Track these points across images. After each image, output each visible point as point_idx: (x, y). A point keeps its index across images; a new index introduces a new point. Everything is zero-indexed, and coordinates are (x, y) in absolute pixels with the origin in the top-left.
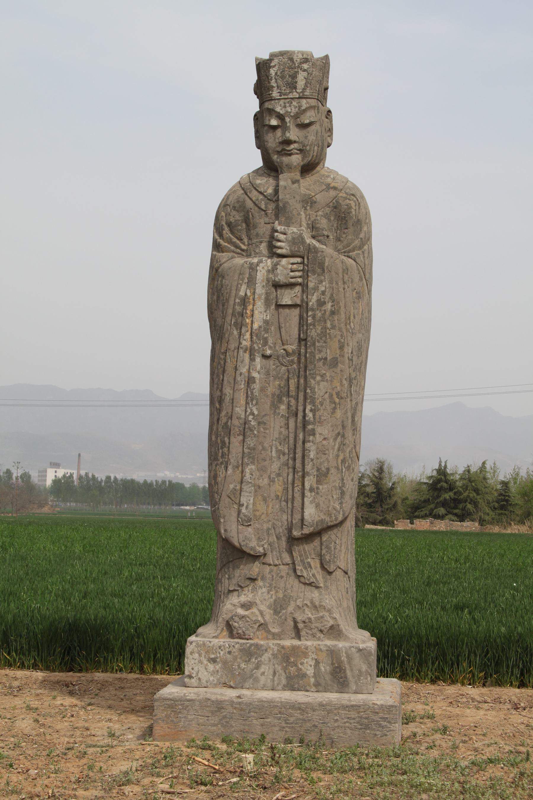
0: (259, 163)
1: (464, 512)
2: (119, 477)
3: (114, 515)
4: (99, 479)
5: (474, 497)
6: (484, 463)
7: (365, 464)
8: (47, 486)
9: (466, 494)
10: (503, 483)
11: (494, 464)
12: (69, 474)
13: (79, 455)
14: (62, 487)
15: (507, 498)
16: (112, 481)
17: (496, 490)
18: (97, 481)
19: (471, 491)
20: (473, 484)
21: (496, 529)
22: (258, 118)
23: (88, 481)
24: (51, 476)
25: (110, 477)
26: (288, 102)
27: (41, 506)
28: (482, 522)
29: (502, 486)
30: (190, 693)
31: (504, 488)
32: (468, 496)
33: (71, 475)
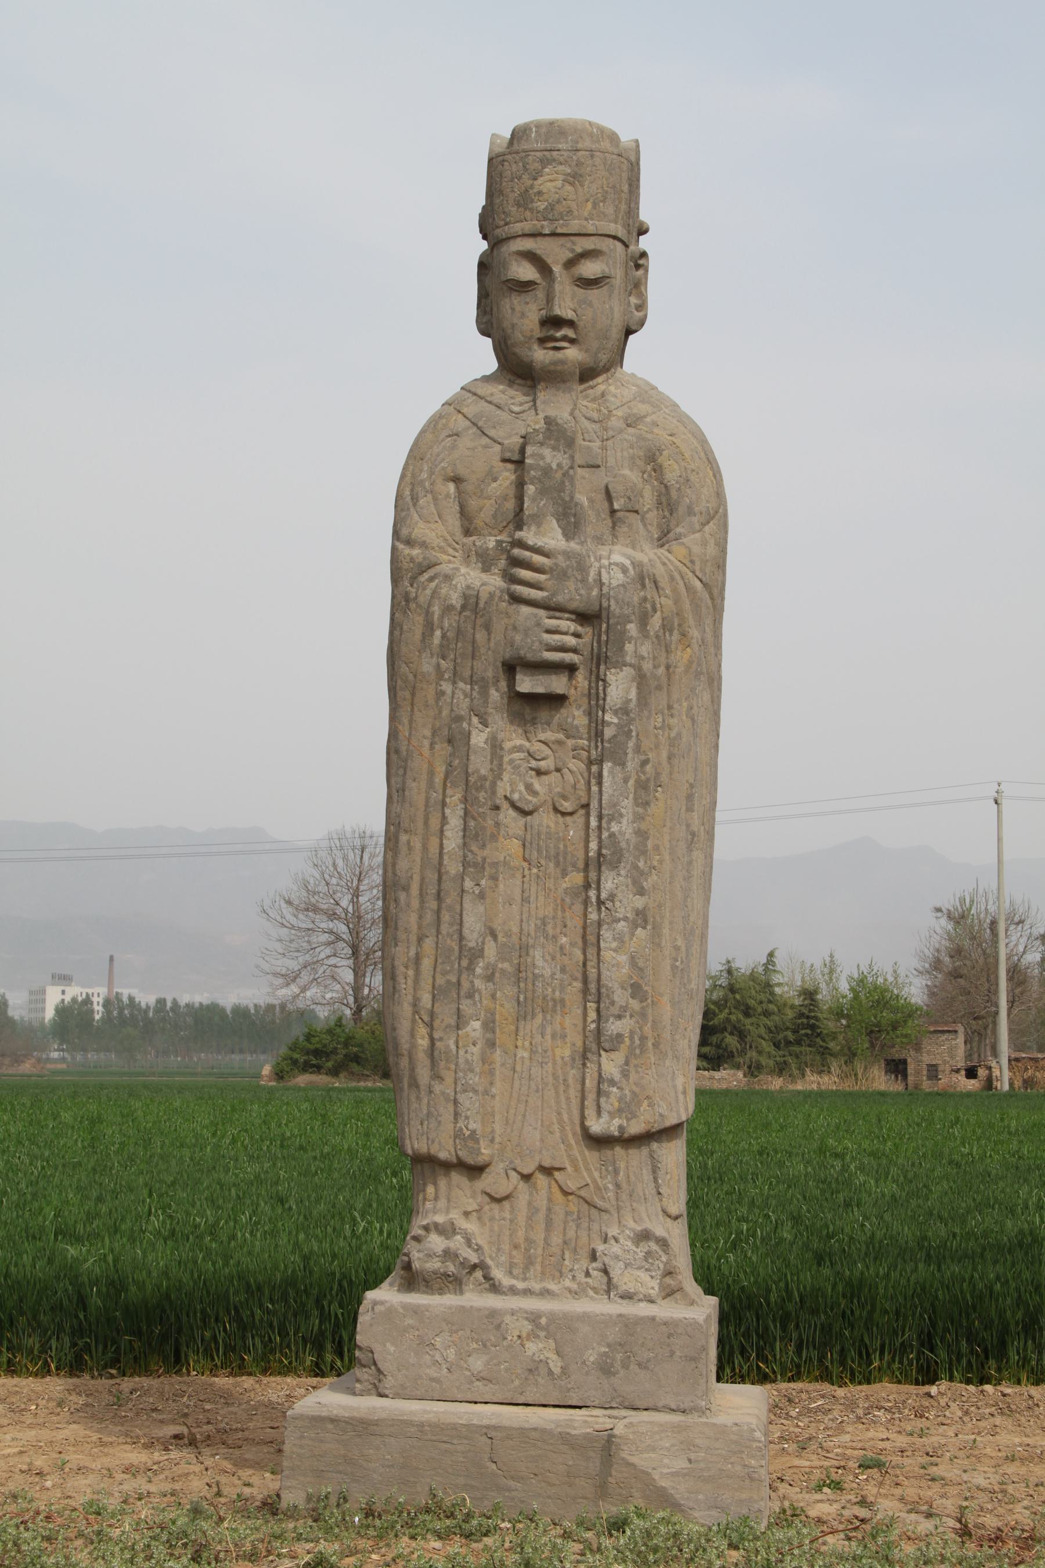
0: (490, 364)
1: (721, 1051)
2: (184, 999)
3: (195, 1074)
4: (143, 1005)
5: (739, 1021)
6: (771, 955)
7: (715, 965)
8: (46, 1021)
9: (722, 1016)
10: (805, 994)
11: (832, 956)
12: (84, 996)
13: (111, 958)
14: (73, 1020)
15: (812, 1021)
16: (168, 1008)
17: (792, 1007)
18: (140, 1009)
19: (733, 1010)
20: (738, 996)
21: (776, 1083)
22: (484, 266)
23: (121, 1010)
24: (54, 997)
25: (165, 1000)
26: (554, 256)
27: (18, 1060)
28: (754, 1070)
29: (805, 999)
30: (366, 1405)
31: (806, 1002)
32: (728, 1020)
33: (88, 1001)
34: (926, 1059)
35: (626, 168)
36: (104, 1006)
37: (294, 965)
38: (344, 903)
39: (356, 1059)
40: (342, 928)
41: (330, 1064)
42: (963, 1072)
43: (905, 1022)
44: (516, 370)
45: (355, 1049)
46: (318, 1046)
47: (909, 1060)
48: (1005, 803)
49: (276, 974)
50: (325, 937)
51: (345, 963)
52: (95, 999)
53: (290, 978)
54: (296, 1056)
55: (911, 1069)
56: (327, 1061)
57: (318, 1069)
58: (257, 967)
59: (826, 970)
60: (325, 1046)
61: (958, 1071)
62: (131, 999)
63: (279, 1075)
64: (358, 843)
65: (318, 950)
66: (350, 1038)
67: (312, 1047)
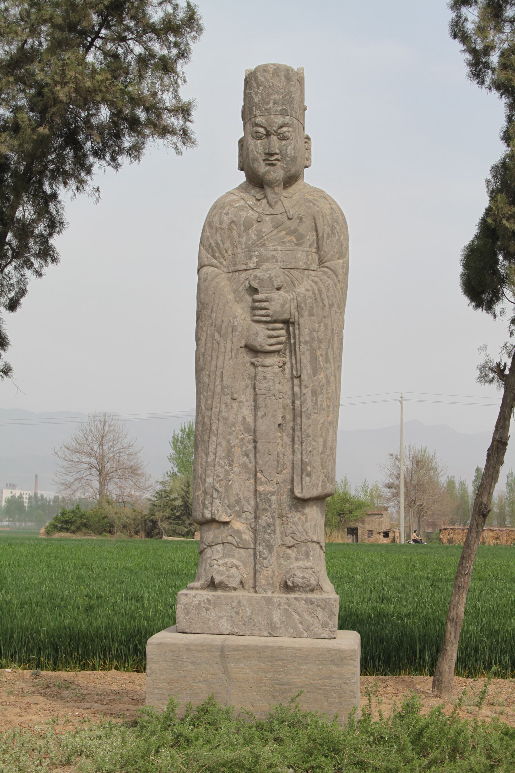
11: (345, 477)
13: (36, 476)
34: (367, 528)
35: (301, 81)
36: (29, 499)
37: (70, 479)
38: (95, 448)
39: (85, 525)
40: (93, 461)
41: (73, 528)
42: (382, 534)
43: (356, 509)
44: (256, 182)
45: (85, 520)
46: (67, 519)
47: (359, 528)
48: (404, 403)
49: (64, 484)
50: (86, 466)
51: (95, 478)
52: (24, 496)
53: (69, 486)
54: (56, 523)
55: (360, 533)
56: (72, 526)
57: (67, 530)
58: (53, 480)
59: (343, 485)
60: (70, 519)
61: (379, 533)
62: (42, 496)
63: (48, 533)
64: (102, 419)
65: (83, 472)
66: (83, 515)
67: (64, 519)
